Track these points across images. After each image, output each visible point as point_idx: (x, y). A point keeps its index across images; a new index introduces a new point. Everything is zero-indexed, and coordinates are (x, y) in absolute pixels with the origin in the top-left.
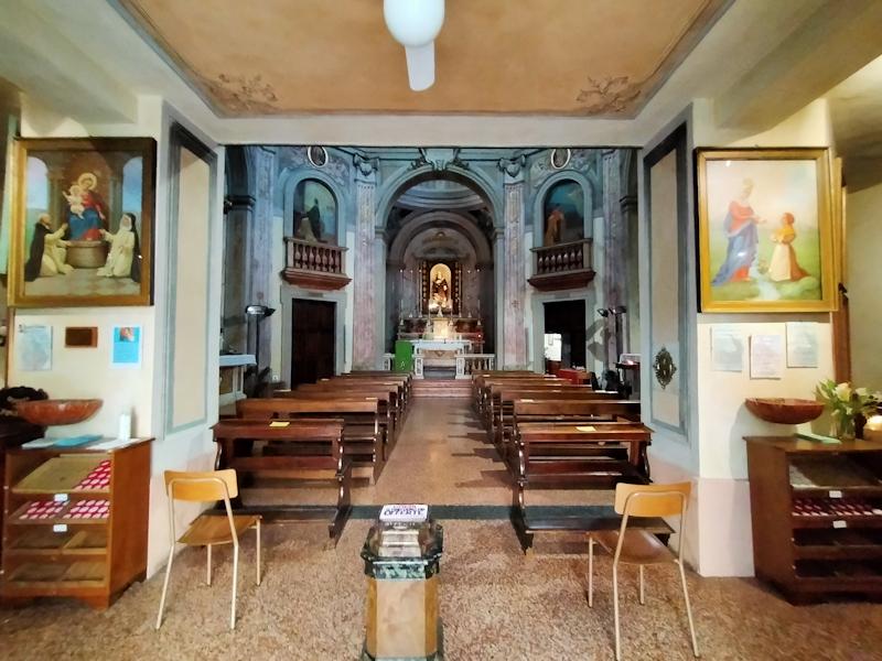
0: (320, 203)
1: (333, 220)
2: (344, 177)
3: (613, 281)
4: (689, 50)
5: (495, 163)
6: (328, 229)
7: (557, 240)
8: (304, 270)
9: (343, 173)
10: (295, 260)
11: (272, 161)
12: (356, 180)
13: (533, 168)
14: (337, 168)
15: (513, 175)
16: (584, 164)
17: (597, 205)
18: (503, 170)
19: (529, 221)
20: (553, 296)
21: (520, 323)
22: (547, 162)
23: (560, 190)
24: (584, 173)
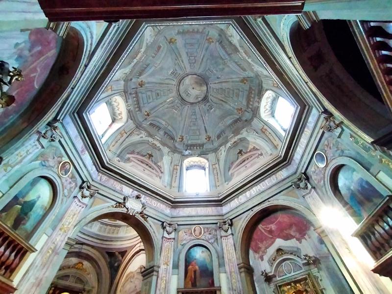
0: (40, 199)
1: (39, 218)
2: (70, 191)
5: (161, 223)
6: (29, 225)
7: (194, 284)
9: (71, 188)
11: (37, 150)
12: (75, 197)
13: (180, 233)
14: (70, 183)
15: (169, 233)
16: (211, 239)
17: (221, 265)
18: (164, 228)
19: (176, 266)
22: (190, 232)
23: (195, 248)
24: (212, 244)
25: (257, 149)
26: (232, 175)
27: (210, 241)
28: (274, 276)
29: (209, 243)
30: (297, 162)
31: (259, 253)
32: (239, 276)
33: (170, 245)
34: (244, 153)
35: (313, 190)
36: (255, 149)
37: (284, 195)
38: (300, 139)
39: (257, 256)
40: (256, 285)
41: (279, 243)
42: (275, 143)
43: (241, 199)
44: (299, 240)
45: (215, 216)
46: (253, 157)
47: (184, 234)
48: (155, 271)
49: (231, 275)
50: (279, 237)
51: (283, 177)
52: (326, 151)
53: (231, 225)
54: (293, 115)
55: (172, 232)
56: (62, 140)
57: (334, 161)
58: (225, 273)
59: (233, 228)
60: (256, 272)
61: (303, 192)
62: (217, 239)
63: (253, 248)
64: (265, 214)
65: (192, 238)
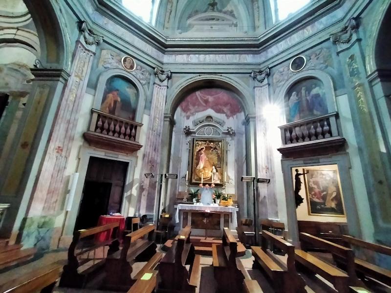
3: (150, 156)
4: (378, 118)
8: (104, 135)
10: (97, 127)
12: (154, 83)
17: (148, 107)
20: (103, 154)
21: (60, 170)
22: (118, 58)
25: (233, 16)
26: (191, 26)
27: (141, 81)
28: (194, 133)
29: (140, 82)
30: (270, 55)
31: (187, 113)
32: (162, 123)
33: (88, 59)
34: (217, 9)
35: (267, 86)
36: (231, 13)
37: (238, 77)
38: (293, 34)
39: (184, 114)
40: (174, 134)
41: (210, 112)
42: (257, 23)
43: (191, 59)
44: (228, 117)
45: (155, 59)
46: (225, 22)
47: (110, 57)
48: (62, 77)
49: (154, 119)
50: (212, 108)
51: (246, 62)
52: (310, 59)
53: (169, 78)
54: (266, 12)
55: (93, 44)
56: (105, 39)
57: (310, 71)
58: (149, 115)
59: (169, 81)
60: (177, 125)
61: (257, 83)
62: (149, 83)
63: (182, 107)
64: (209, 85)
65: (120, 67)
